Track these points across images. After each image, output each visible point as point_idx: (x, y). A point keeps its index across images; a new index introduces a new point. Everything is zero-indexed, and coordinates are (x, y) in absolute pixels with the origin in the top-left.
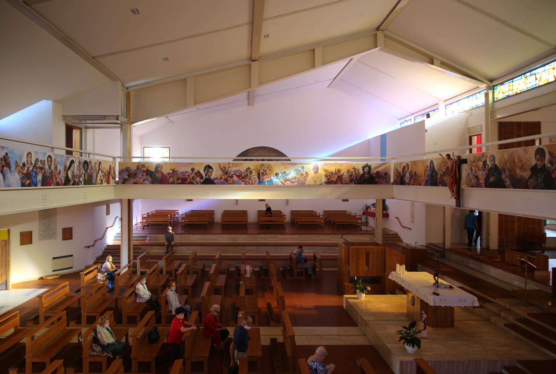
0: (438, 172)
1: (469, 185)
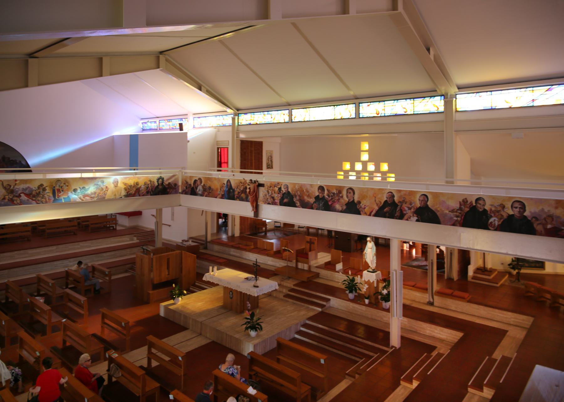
0: (235, 189)
1: (266, 202)
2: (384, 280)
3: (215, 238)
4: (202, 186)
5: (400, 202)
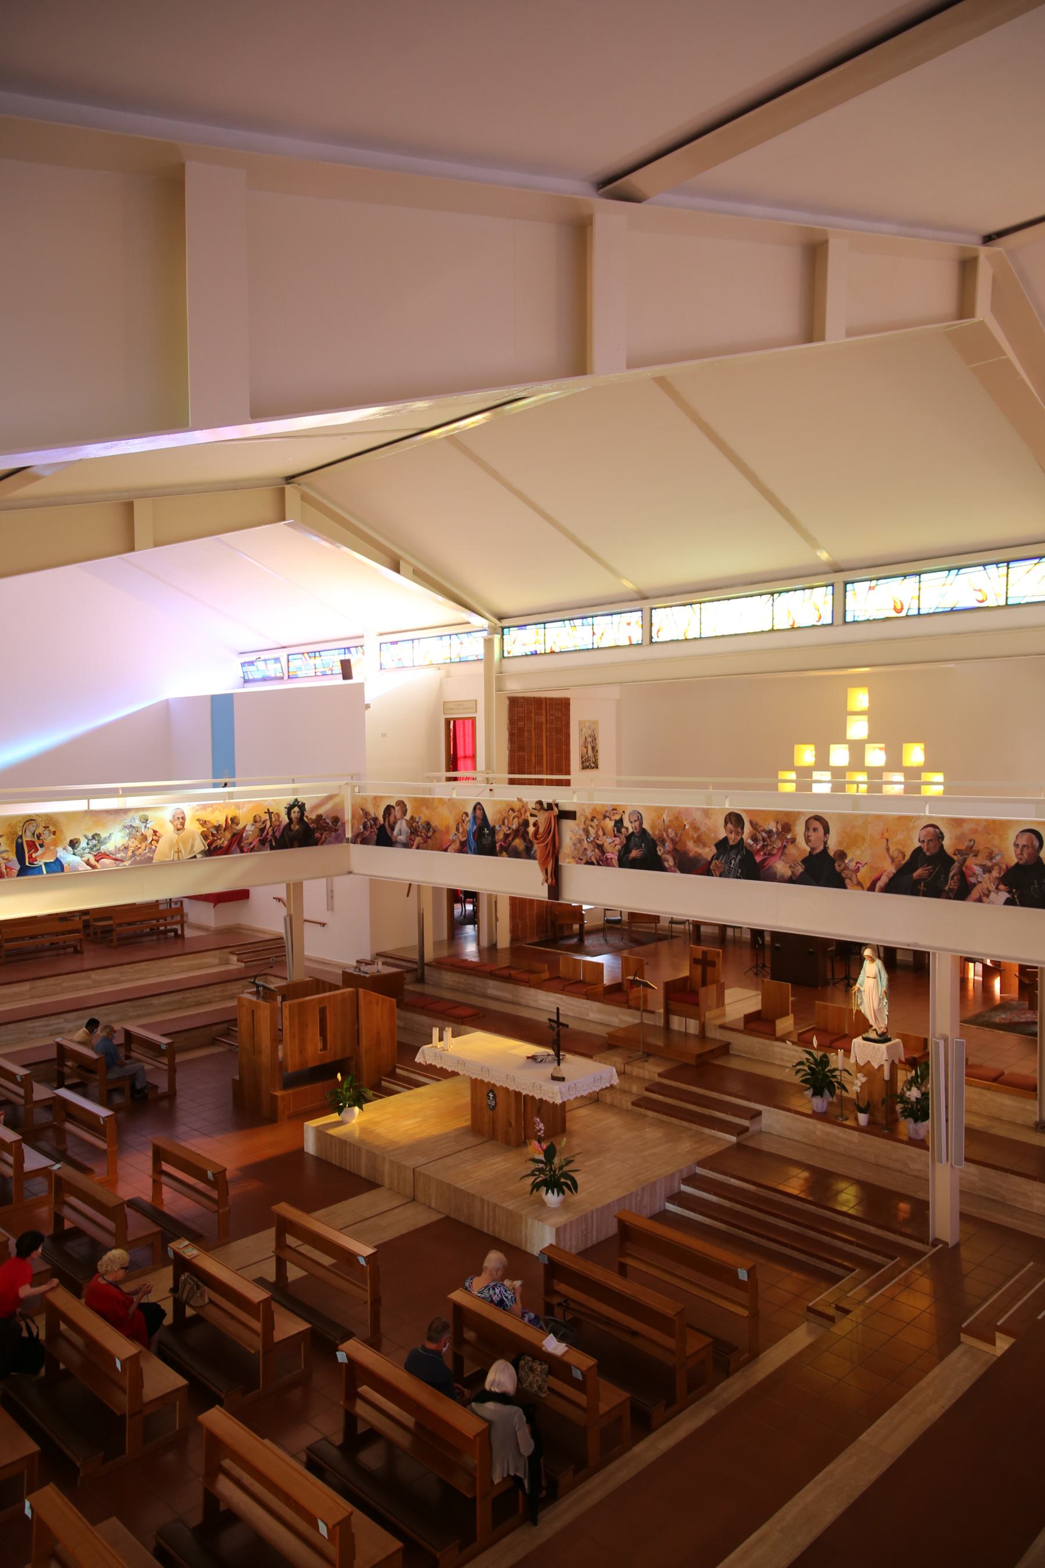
0: (497, 827)
1: (581, 860)
2: (912, 1063)
3: (445, 953)
4: (406, 820)
5: (958, 852)
